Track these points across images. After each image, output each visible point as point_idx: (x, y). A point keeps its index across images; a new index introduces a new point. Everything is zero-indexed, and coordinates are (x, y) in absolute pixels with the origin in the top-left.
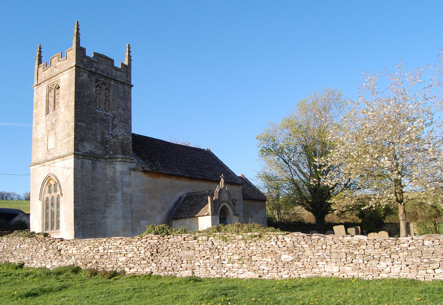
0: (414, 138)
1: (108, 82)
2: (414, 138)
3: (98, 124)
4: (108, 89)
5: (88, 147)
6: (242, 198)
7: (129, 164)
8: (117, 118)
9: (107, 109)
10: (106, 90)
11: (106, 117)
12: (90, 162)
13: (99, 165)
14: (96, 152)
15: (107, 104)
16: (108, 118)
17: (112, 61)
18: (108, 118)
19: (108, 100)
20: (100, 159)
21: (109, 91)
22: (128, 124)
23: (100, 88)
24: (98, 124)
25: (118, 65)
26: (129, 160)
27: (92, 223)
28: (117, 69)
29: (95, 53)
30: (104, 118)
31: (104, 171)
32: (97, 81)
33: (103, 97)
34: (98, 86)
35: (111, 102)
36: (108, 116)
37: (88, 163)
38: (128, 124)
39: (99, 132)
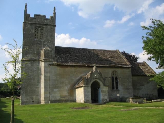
0: (14, 60)
1: (41, 26)
2: (14, 60)
3: (35, 46)
4: (42, 29)
5: (30, 56)
6: (131, 75)
7: (49, 62)
8: (46, 41)
9: (42, 38)
10: (41, 30)
11: (40, 42)
12: (30, 63)
13: (35, 64)
14: (34, 58)
15: (42, 36)
16: (41, 42)
17: (45, 17)
18: (41, 42)
19: (42, 34)
20: (35, 61)
21: (43, 30)
22: (53, 43)
23: (38, 30)
24: (35, 46)
25: (48, 17)
26: (48, 61)
27: (30, 90)
28: (47, 19)
29: (35, 15)
30: (39, 42)
31: (38, 67)
32: (36, 27)
33: (39, 33)
34: (37, 29)
35: (44, 35)
36: (42, 41)
37: (29, 64)
38: (53, 43)
39: (36, 49)
